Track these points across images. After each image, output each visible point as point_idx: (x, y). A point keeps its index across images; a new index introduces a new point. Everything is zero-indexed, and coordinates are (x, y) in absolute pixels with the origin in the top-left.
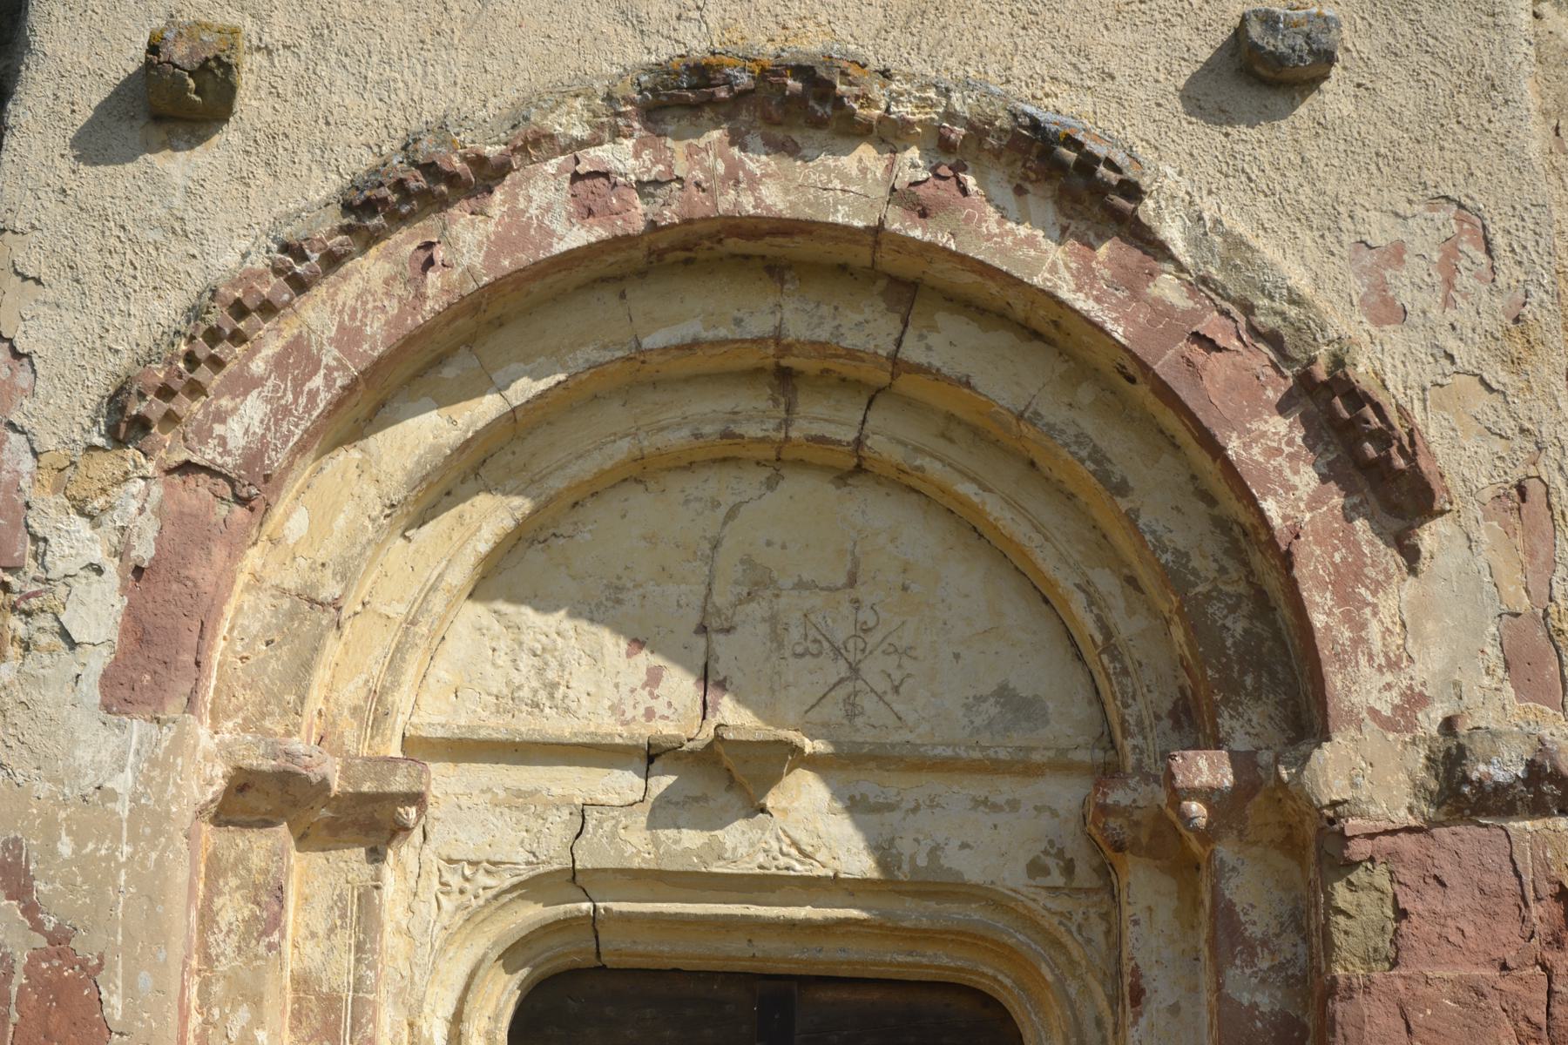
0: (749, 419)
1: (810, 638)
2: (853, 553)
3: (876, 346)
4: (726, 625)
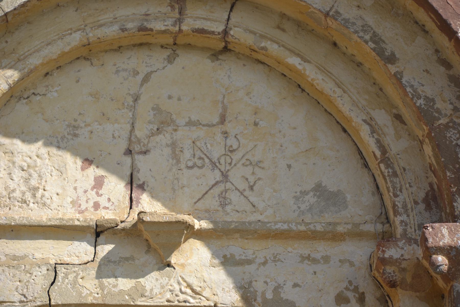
0: (156, 19)
2: (223, 102)
4: (144, 149)
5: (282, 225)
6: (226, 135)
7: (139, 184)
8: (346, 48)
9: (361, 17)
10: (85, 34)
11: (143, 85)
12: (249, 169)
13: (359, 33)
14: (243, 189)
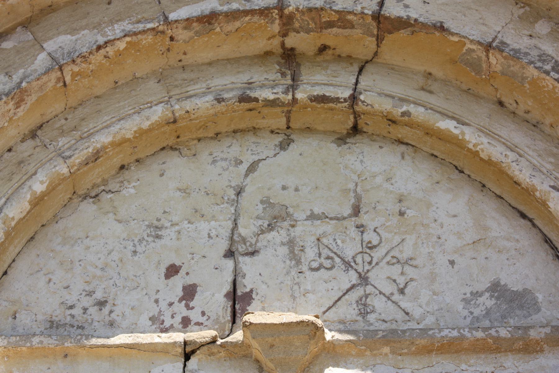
0: (262, 86)
1: (324, 256)
2: (355, 191)
3: (362, 8)
4: (250, 250)
5: (449, 332)
6: (362, 229)
7: (245, 292)
8: (517, 103)
9: (535, 47)
10: (169, 106)
11: (248, 175)
12: (397, 269)
13: (536, 63)
14: (390, 292)
